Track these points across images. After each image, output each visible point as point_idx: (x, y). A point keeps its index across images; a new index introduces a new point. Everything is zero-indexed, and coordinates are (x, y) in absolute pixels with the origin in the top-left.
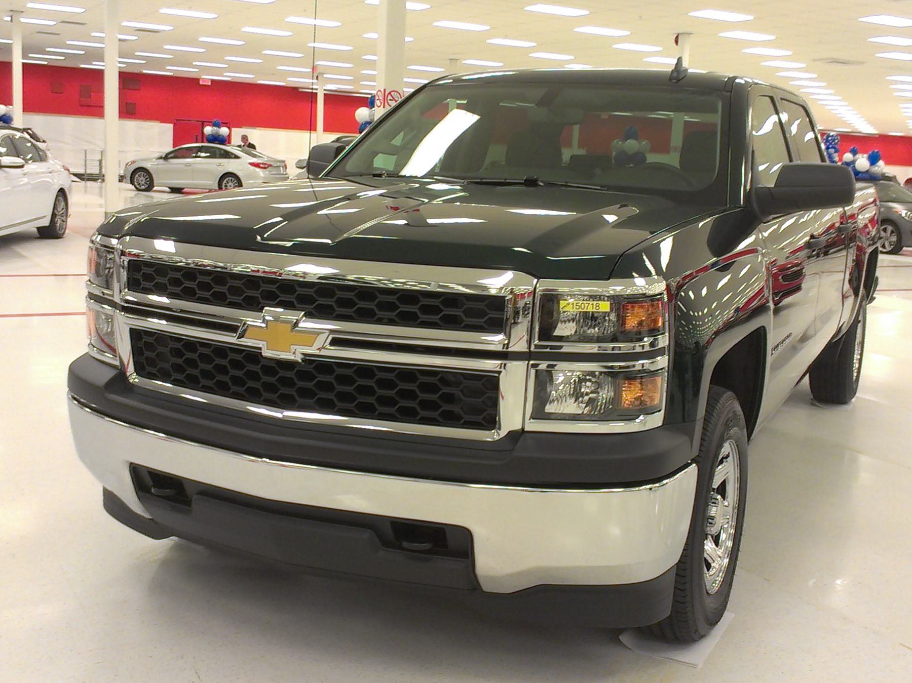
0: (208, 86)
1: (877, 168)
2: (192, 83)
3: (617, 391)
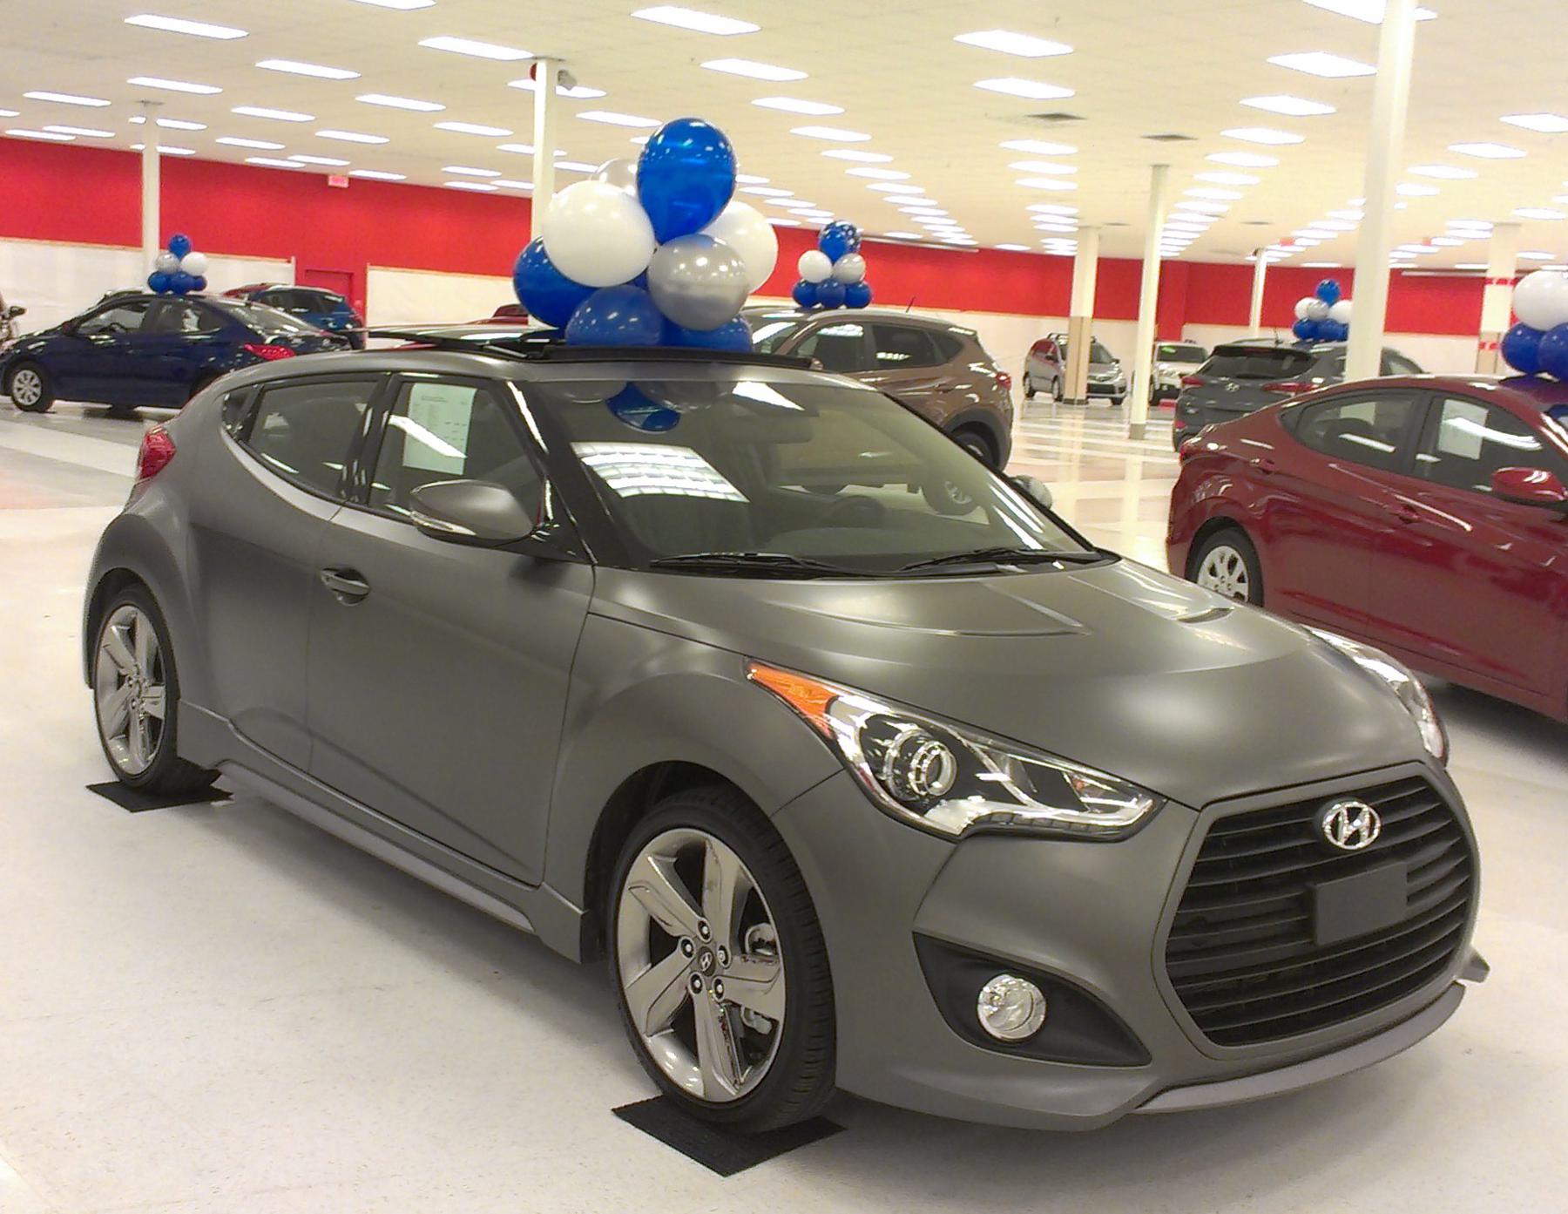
0: (341, 189)
1: (702, 261)
2: (313, 182)
3: (999, 1043)
